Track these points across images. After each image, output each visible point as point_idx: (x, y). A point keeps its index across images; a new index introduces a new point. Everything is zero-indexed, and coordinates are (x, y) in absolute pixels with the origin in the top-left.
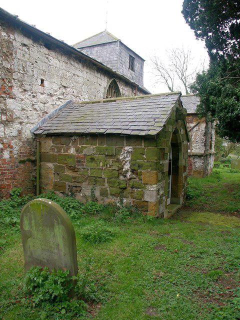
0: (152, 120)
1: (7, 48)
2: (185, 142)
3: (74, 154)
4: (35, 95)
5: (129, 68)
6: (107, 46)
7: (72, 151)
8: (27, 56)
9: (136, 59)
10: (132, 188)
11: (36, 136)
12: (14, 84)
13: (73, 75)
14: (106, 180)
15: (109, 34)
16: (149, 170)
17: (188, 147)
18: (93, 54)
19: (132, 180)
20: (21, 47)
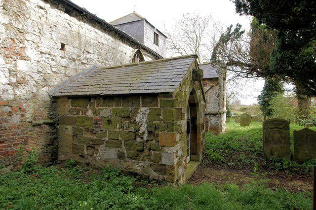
0: (168, 80)
1: (19, 8)
2: (202, 102)
3: (91, 116)
4: (54, 58)
5: (154, 43)
6: (135, 24)
7: (90, 113)
8: (43, 19)
9: (160, 36)
10: (150, 150)
11: (55, 99)
12: (28, 46)
13: (97, 43)
14: (123, 142)
15: (137, 15)
16: (166, 131)
17: (205, 107)
18: (124, 30)
19: (150, 142)
20: (37, 9)
